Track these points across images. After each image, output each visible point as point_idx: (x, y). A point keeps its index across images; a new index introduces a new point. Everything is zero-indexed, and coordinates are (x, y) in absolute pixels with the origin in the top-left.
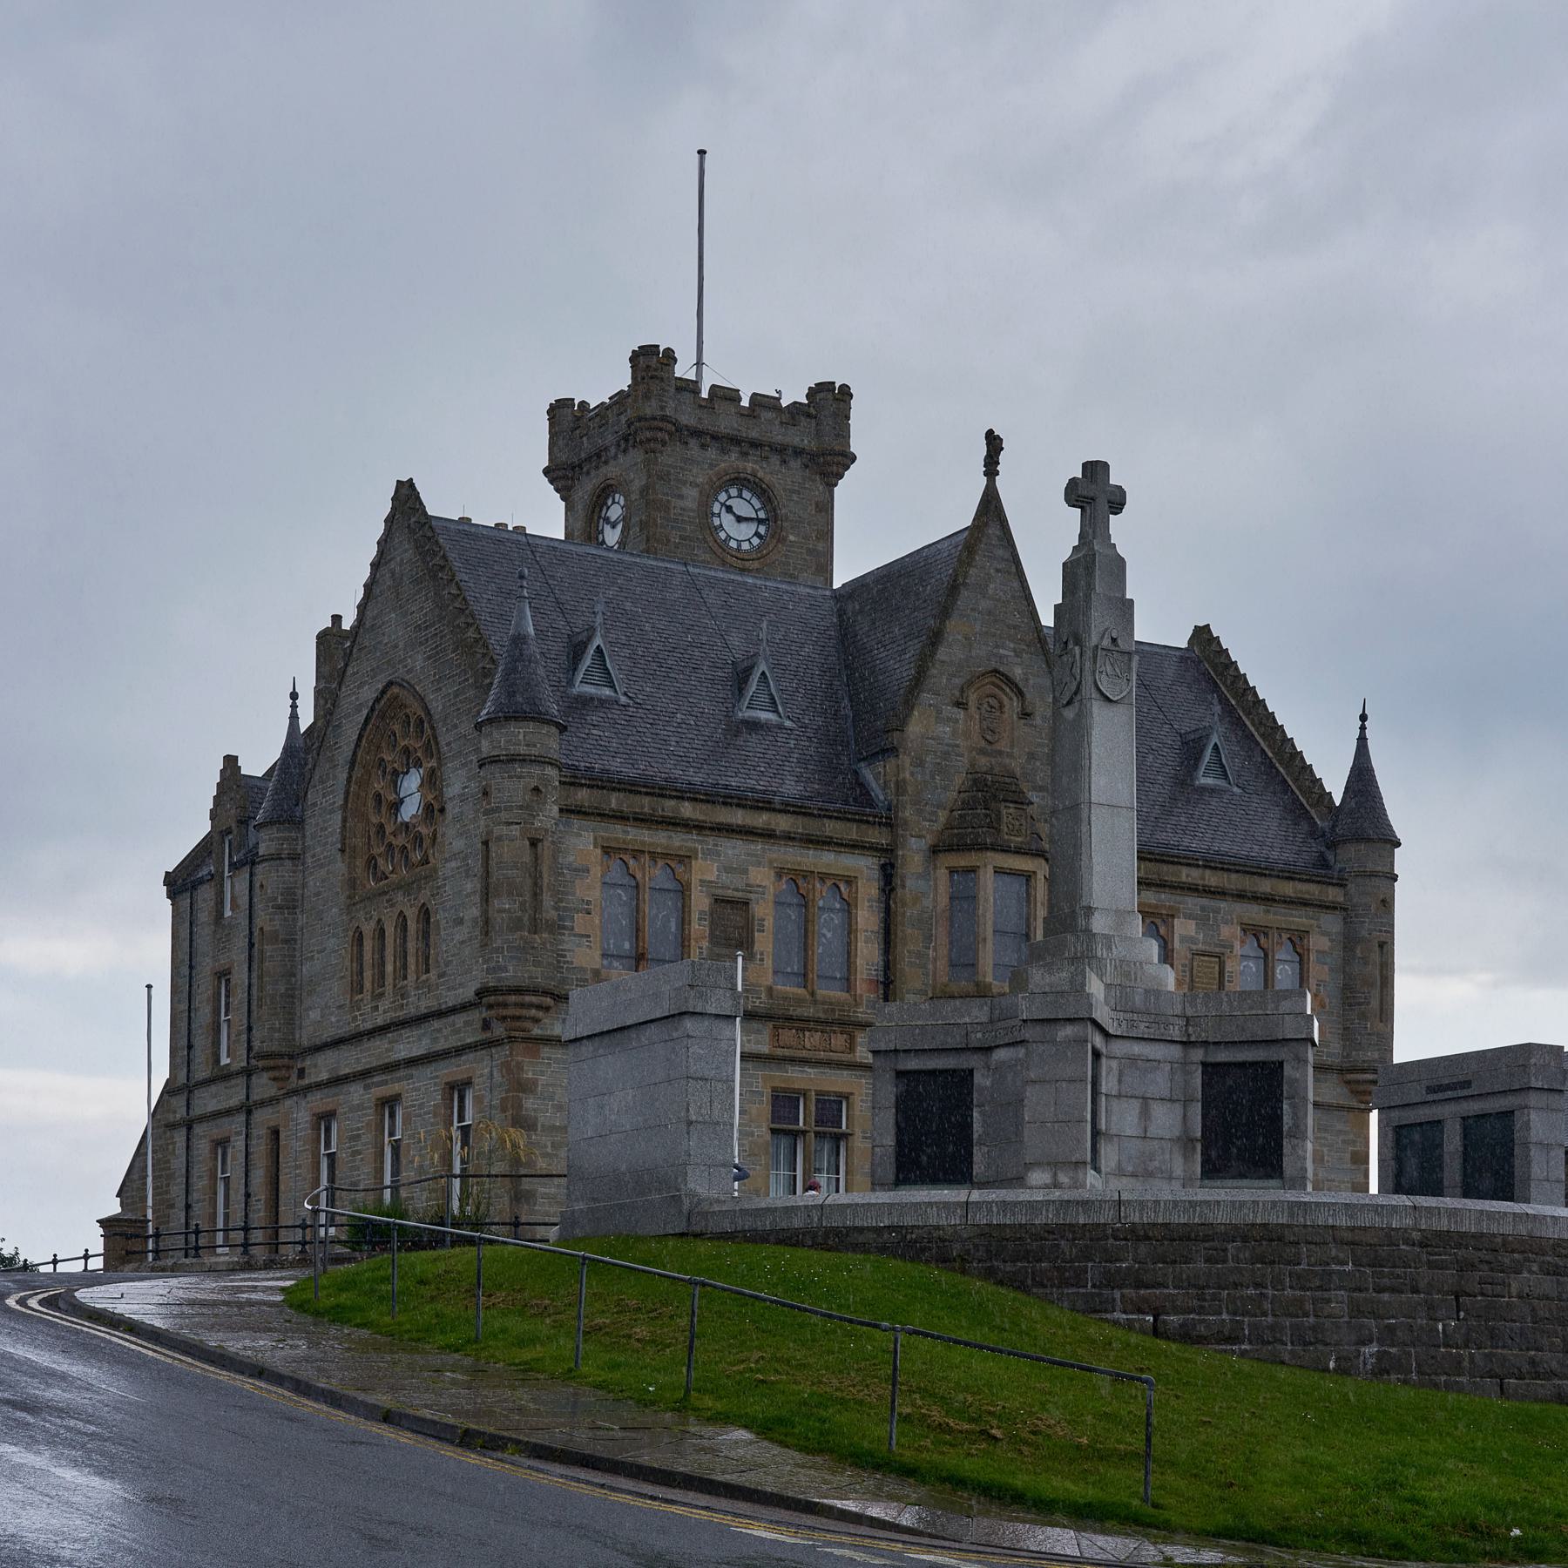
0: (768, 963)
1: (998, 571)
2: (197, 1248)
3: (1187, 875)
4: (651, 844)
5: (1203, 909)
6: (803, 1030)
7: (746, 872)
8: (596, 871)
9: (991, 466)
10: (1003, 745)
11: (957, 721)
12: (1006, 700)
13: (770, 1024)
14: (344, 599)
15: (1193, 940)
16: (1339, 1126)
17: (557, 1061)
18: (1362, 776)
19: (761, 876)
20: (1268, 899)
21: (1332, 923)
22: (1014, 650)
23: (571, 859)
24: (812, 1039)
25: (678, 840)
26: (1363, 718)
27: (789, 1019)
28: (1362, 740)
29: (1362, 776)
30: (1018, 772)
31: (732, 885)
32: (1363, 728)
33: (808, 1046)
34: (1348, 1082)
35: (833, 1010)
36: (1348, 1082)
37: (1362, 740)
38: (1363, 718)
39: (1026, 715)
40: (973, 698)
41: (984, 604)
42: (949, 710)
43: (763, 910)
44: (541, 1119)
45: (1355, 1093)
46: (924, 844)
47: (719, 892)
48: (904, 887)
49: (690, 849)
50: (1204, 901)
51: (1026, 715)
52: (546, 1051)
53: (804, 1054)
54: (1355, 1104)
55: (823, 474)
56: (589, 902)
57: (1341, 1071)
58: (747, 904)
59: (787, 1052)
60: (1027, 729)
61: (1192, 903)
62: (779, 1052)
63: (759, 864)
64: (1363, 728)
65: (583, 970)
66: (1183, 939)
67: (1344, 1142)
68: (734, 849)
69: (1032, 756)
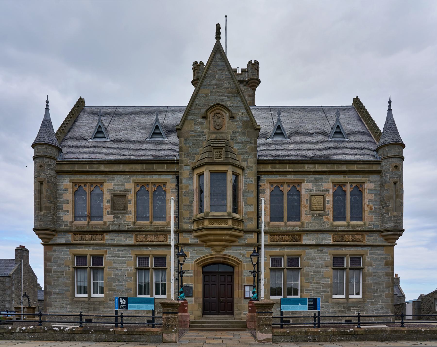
0: (133, 214)
1: (219, 70)
2: (122, 324)
3: (306, 167)
4: (90, 180)
5: (315, 179)
6: (147, 235)
7: (124, 185)
8: (70, 190)
9: (218, 36)
10: (225, 129)
11: (203, 124)
12: (224, 114)
13: (134, 235)
14: (401, 285)
15: (310, 190)
16: (379, 252)
17: (58, 251)
18: (390, 121)
19: (130, 186)
20: (343, 173)
21: (375, 178)
22: (227, 96)
23: (62, 187)
24: (150, 238)
25: (99, 178)
26: (390, 102)
27: (140, 232)
28: (390, 110)
29: (390, 121)
30: (229, 138)
31: (119, 190)
32: (390, 106)
33: (149, 240)
34: (383, 236)
35: (158, 228)
36: (383, 236)
37: (390, 110)
38: (390, 102)
39: (232, 118)
40: (210, 115)
41: (214, 82)
42: (199, 120)
43: (131, 197)
44: (53, 269)
45: (386, 240)
46: (189, 168)
47: (113, 192)
48: (182, 183)
49: (104, 180)
50: (317, 176)
51: (232, 118)
52: (54, 248)
53: (147, 243)
54: (386, 243)
55: (253, 89)
56: (68, 200)
57: (380, 232)
58: (125, 195)
59: (141, 243)
60: (233, 123)
61: (312, 177)
62: (137, 243)
63: (129, 182)
64: (390, 106)
65: (66, 222)
66: (306, 190)
67: (381, 258)
68: (120, 178)
69: (234, 132)
